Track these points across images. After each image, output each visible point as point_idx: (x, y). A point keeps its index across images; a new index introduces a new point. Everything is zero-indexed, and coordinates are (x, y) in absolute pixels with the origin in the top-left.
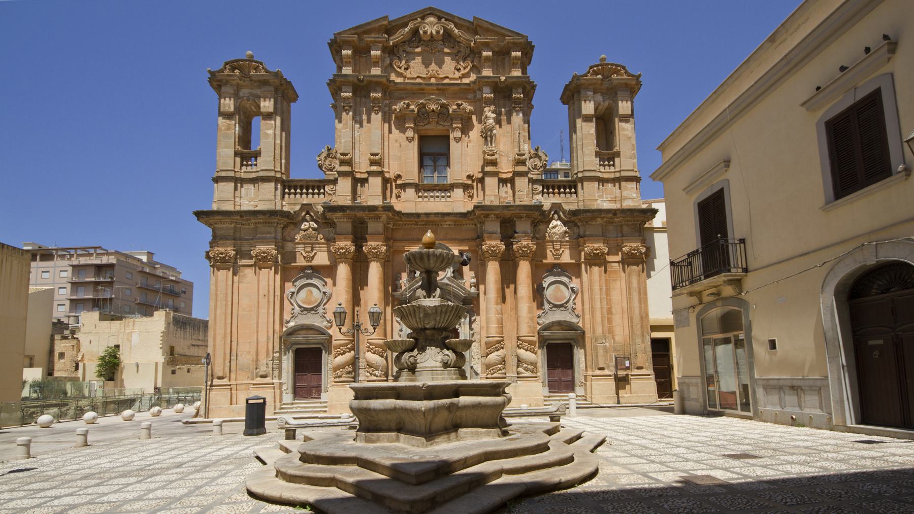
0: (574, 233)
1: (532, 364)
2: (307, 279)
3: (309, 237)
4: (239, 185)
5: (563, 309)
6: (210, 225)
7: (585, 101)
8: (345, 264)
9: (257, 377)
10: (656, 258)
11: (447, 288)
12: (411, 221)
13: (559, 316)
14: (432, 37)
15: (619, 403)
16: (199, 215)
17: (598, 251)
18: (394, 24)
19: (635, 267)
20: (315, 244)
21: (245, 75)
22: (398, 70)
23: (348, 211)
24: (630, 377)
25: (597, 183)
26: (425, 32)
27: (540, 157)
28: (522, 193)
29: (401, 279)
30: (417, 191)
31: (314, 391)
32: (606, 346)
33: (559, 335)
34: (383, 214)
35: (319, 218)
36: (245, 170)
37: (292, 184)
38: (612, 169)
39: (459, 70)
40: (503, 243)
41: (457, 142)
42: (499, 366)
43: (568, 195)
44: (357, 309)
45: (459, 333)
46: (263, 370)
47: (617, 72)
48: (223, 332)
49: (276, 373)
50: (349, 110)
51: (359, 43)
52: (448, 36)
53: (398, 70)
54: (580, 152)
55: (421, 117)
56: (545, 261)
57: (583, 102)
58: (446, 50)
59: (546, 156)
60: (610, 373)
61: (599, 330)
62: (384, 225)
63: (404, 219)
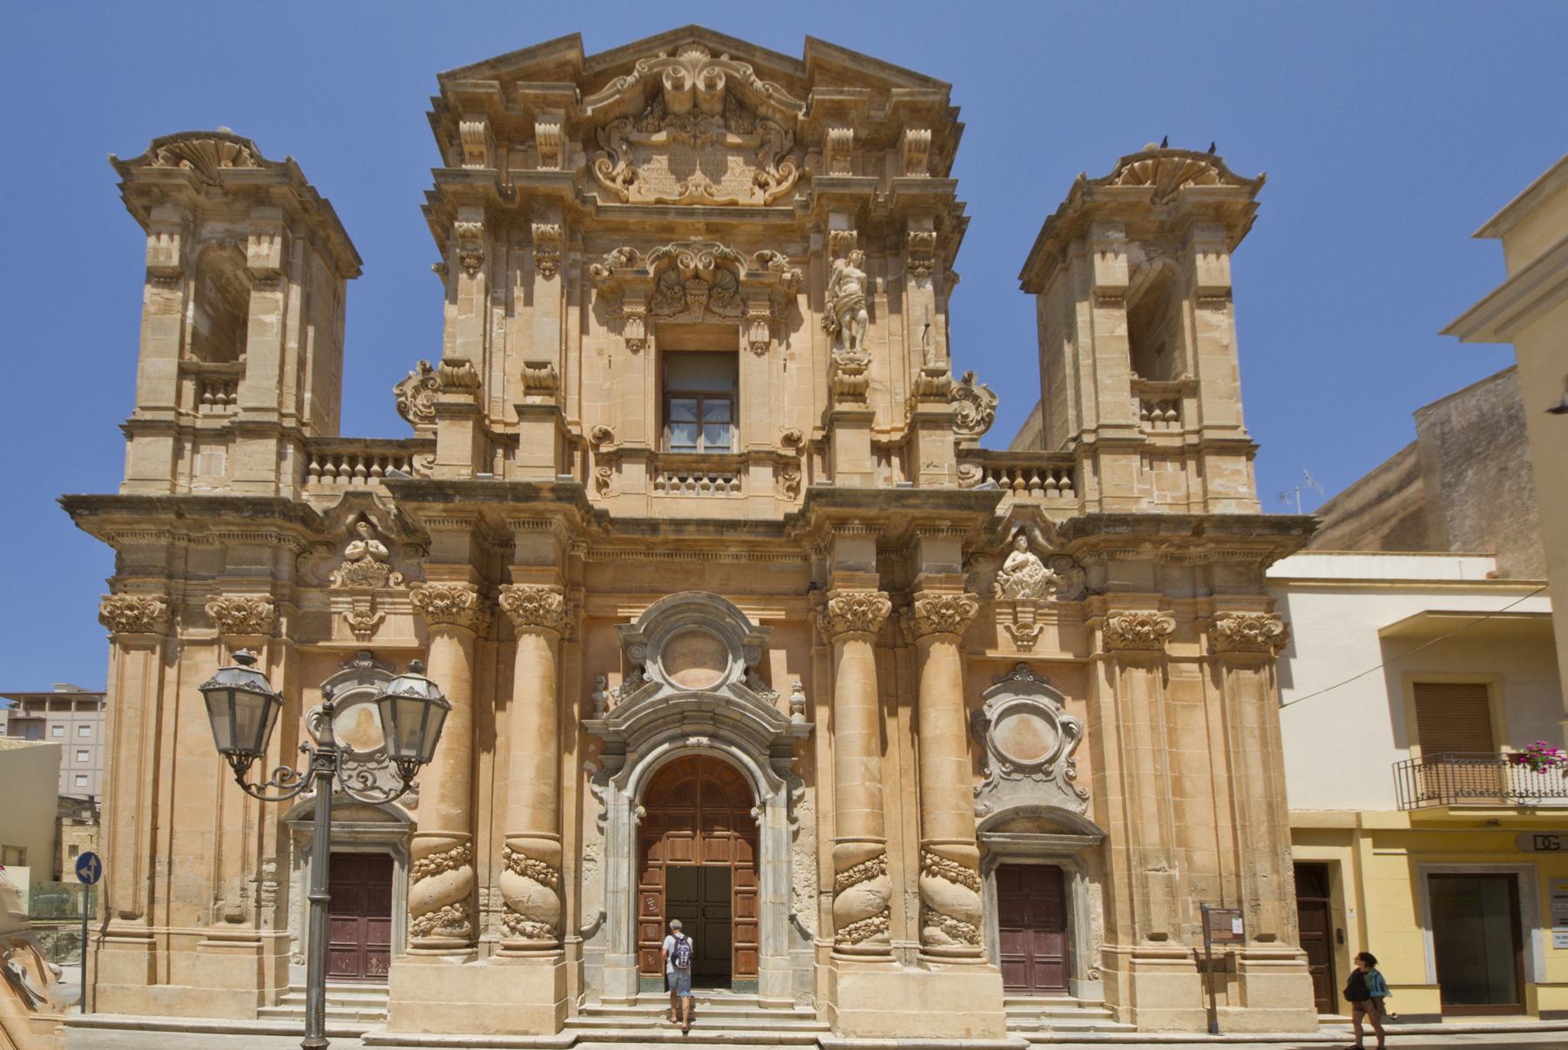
0: (1070, 586)
2: (361, 683)
3: (365, 578)
4: (188, 446)
5: (1040, 776)
6: (110, 539)
7: (1103, 254)
8: (451, 637)
9: (218, 920)
10: (1294, 656)
11: (726, 713)
12: (635, 542)
13: (1028, 794)
15: (1213, 1029)
16: (75, 506)
17: (1147, 628)
18: (597, 68)
19: (1248, 674)
20: (382, 594)
21: (205, 177)
22: (608, 183)
23: (457, 498)
24: (1238, 960)
26: (678, 86)
27: (975, 399)
28: (936, 471)
29: (606, 688)
30: (654, 471)
31: (374, 961)
32: (1170, 877)
33: (1032, 844)
34: (556, 512)
35: (390, 529)
36: (209, 413)
37: (329, 450)
38: (1175, 427)
39: (763, 186)
40: (886, 593)
41: (758, 355)
42: (877, 921)
43: (1054, 493)
44: (485, 759)
45: (758, 828)
46: (231, 903)
47: (1197, 175)
48: (134, 803)
49: (268, 912)
50: (476, 269)
51: (506, 108)
52: (737, 103)
53: (608, 183)
55: (664, 295)
56: (990, 653)
57: (1097, 257)
58: (732, 139)
59: (992, 396)
61: (1152, 836)
62: (564, 551)
63: (616, 535)
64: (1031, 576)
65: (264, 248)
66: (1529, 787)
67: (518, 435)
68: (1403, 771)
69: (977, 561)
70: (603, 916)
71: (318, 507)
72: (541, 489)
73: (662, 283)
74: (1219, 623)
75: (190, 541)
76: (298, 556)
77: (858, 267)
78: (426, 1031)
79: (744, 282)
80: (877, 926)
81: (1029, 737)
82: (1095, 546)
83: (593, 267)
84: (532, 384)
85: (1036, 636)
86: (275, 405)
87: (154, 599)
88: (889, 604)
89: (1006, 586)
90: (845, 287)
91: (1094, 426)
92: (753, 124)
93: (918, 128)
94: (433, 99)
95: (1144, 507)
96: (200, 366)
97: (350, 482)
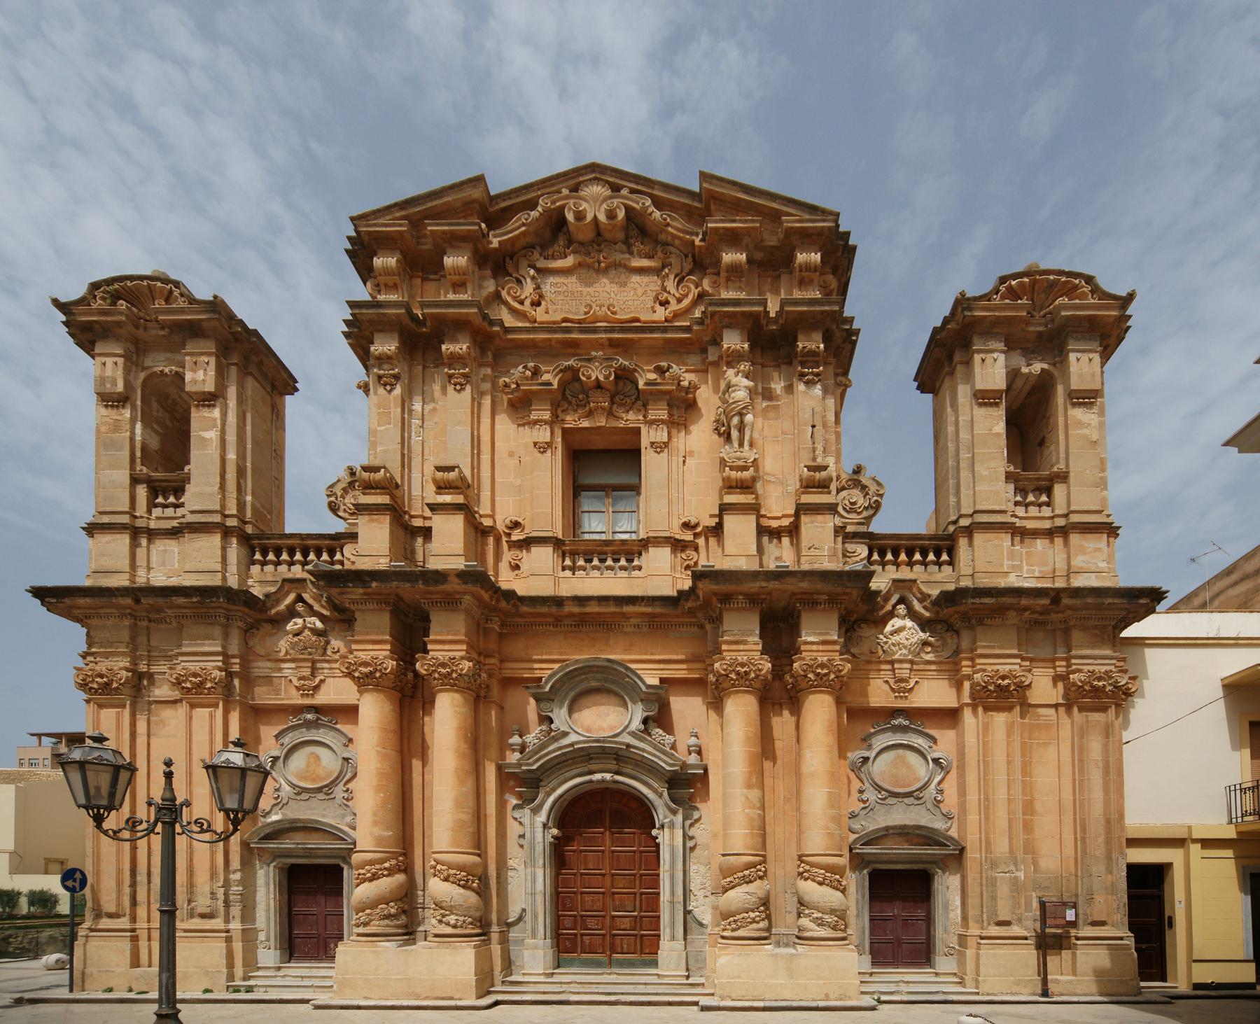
1: (832, 911)
5: (910, 800)
9: (192, 917)
13: (901, 815)
14: (599, 234)
15: (1045, 993)
17: (1006, 682)
25: (1009, 536)
26: (580, 216)
28: (817, 552)
34: (465, 593)
38: (1046, 512)
39: (664, 304)
40: (766, 657)
42: (752, 915)
47: (1071, 291)
49: (236, 911)
54: (965, 475)
55: (570, 403)
60: (1026, 934)
61: (1001, 846)
62: (478, 625)
63: (525, 609)
64: (907, 639)
65: (200, 375)
66: (1248, 809)
67: (431, 527)
68: (1233, 793)
69: (860, 627)
70: (524, 910)
71: (257, 591)
72: (449, 575)
73: (568, 392)
74: (1071, 676)
75: (150, 621)
76: (246, 631)
77: (747, 378)
78: (366, 998)
79: (645, 391)
80: (754, 919)
81: (904, 770)
82: (965, 613)
83: (501, 380)
84: (443, 485)
85: (912, 689)
86: (218, 507)
87: (121, 669)
88: (770, 665)
89: (886, 647)
90: (733, 395)
91: (971, 511)
92: (654, 249)
93: (808, 251)
94: (349, 238)
95: (1013, 581)
96: (150, 476)
97: (289, 570)
